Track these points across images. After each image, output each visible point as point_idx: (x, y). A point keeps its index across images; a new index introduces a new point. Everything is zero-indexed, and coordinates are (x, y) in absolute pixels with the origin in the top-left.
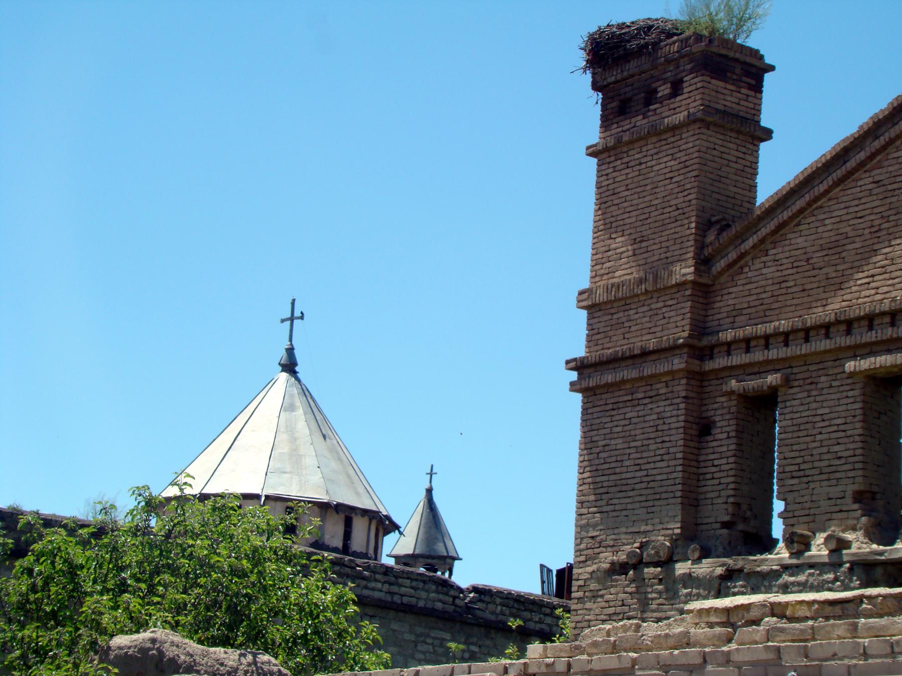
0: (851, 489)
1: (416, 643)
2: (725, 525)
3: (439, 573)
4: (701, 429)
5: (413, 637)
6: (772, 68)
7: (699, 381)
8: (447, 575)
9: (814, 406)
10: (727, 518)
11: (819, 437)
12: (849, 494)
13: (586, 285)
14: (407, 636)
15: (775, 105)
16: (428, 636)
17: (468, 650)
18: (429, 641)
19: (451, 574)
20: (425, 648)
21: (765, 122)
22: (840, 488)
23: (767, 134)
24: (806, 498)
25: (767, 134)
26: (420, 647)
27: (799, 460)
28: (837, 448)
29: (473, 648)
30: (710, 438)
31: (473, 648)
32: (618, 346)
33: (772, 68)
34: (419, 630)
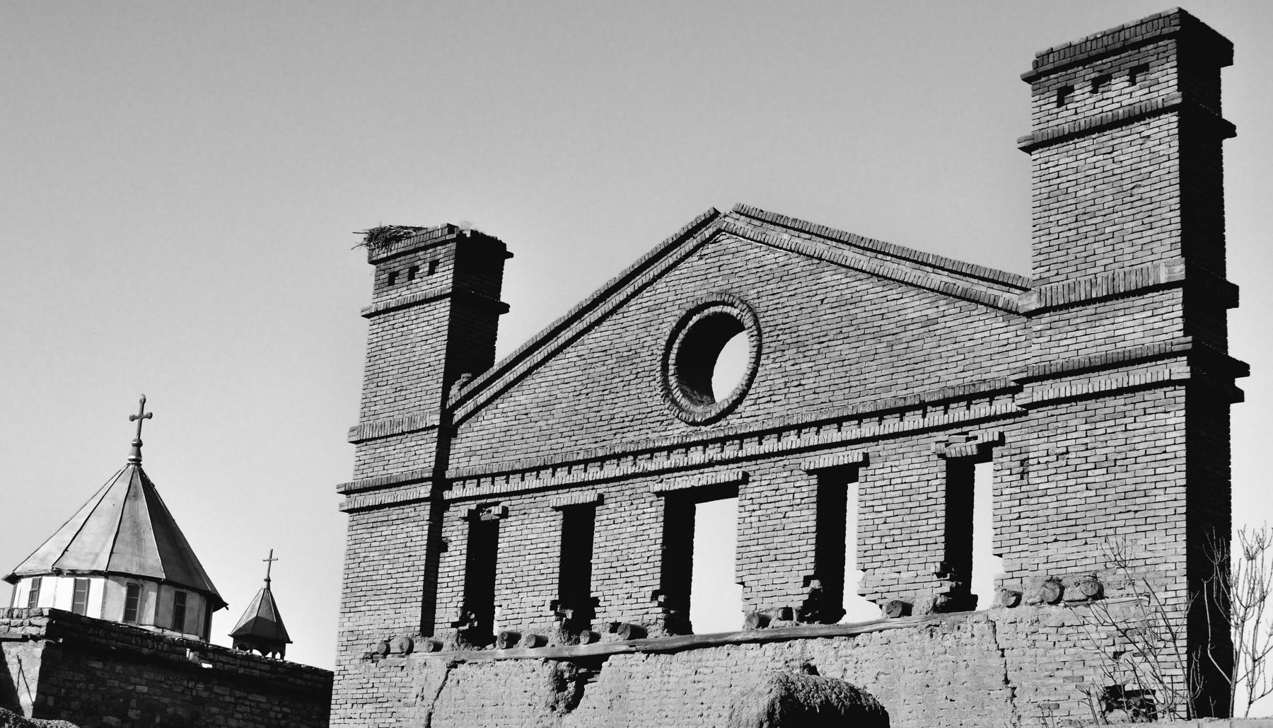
0: (549, 599)
1: (236, 704)
2: (454, 625)
3: (270, 655)
4: (436, 546)
5: (233, 700)
6: (511, 255)
7: (439, 506)
8: (278, 656)
9: (525, 532)
10: (457, 619)
11: (528, 557)
12: (548, 604)
13: (356, 423)
14: (227, 699)
15: (515, 284)
16: (246, 699)
17: (281, 712)
18: (247, 703)
19: (282, 656)
20: (243, 709)
21: (504, 298)
22: (541, 598)
23: (505, 308)
24: (517, 605)
25: (505, 308)
26: (238, 709)
27: (513, 575)
28: (541, 566)
29: (285, 709)
30: (446, 554)
31: (285, 709)
32: (378, 474)
33: (511, 255)
34: (238, 693)
